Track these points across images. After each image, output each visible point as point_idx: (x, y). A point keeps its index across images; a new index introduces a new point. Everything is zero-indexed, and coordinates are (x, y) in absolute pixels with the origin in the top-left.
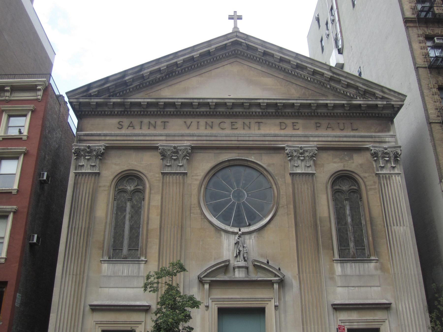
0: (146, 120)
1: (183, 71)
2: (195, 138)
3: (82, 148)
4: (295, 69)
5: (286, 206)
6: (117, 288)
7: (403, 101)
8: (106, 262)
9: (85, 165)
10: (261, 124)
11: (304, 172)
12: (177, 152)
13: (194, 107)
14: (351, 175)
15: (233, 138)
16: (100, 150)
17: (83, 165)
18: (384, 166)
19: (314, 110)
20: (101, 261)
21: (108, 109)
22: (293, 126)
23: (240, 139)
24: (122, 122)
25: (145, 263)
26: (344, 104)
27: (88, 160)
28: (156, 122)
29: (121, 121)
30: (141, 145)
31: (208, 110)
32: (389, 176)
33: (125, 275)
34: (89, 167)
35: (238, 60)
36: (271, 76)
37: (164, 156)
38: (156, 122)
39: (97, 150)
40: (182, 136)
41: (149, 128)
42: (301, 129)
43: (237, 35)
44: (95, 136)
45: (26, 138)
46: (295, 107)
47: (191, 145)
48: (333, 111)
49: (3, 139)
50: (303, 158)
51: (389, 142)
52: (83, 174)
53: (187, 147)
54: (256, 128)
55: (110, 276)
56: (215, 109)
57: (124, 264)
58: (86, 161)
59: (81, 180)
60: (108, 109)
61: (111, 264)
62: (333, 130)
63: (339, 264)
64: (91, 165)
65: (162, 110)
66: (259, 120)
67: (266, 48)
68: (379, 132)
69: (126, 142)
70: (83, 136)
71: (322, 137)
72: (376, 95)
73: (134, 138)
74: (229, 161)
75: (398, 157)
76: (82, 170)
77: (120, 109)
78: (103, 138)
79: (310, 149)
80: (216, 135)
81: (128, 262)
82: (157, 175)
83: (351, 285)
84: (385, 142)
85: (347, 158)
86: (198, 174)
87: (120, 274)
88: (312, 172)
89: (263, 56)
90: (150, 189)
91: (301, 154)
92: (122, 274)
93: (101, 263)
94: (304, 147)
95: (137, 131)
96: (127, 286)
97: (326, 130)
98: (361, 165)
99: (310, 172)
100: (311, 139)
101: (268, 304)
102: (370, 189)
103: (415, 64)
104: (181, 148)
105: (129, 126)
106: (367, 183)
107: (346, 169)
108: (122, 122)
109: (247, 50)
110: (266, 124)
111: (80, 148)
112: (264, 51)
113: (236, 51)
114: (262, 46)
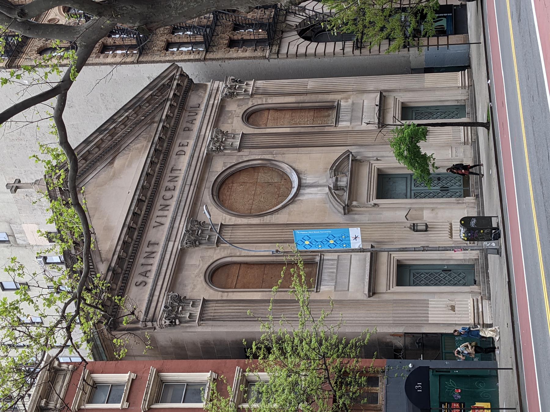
2: (179, 218)
4: (112, 139)
5: (274, 155)
7: (179, 67)
8: (319, 287)
15: (187, 188)
20: (317, 292)
22: (169, 190)
23: (189, 182)
26: (170, 105)
31: (146, 204)
33: (335, 270)
37: (218, 150)
40: (152, 295)
41: (166, 216)
45: (134, 375)
49: (127, 401)
50: (181, 307)
51: (219, 85)
52: (201, 313)
55: (336, 282)
57: (323, 272)
61: (322, 283)
64: (192, 306)
65: (123, 272)
69: (167, 277)
70: (147, 317)
71: (205, 115)
72: (166, 83)
73: (164, 269)
79: (214, 133)
82: (218, 251)
84: (218, 88)
86: (224, 218)
89: (86, 161)
95: (182, 174)
100: (203, 133)
102: (266, 101)
103: (132, 63)
110: (174, 165)
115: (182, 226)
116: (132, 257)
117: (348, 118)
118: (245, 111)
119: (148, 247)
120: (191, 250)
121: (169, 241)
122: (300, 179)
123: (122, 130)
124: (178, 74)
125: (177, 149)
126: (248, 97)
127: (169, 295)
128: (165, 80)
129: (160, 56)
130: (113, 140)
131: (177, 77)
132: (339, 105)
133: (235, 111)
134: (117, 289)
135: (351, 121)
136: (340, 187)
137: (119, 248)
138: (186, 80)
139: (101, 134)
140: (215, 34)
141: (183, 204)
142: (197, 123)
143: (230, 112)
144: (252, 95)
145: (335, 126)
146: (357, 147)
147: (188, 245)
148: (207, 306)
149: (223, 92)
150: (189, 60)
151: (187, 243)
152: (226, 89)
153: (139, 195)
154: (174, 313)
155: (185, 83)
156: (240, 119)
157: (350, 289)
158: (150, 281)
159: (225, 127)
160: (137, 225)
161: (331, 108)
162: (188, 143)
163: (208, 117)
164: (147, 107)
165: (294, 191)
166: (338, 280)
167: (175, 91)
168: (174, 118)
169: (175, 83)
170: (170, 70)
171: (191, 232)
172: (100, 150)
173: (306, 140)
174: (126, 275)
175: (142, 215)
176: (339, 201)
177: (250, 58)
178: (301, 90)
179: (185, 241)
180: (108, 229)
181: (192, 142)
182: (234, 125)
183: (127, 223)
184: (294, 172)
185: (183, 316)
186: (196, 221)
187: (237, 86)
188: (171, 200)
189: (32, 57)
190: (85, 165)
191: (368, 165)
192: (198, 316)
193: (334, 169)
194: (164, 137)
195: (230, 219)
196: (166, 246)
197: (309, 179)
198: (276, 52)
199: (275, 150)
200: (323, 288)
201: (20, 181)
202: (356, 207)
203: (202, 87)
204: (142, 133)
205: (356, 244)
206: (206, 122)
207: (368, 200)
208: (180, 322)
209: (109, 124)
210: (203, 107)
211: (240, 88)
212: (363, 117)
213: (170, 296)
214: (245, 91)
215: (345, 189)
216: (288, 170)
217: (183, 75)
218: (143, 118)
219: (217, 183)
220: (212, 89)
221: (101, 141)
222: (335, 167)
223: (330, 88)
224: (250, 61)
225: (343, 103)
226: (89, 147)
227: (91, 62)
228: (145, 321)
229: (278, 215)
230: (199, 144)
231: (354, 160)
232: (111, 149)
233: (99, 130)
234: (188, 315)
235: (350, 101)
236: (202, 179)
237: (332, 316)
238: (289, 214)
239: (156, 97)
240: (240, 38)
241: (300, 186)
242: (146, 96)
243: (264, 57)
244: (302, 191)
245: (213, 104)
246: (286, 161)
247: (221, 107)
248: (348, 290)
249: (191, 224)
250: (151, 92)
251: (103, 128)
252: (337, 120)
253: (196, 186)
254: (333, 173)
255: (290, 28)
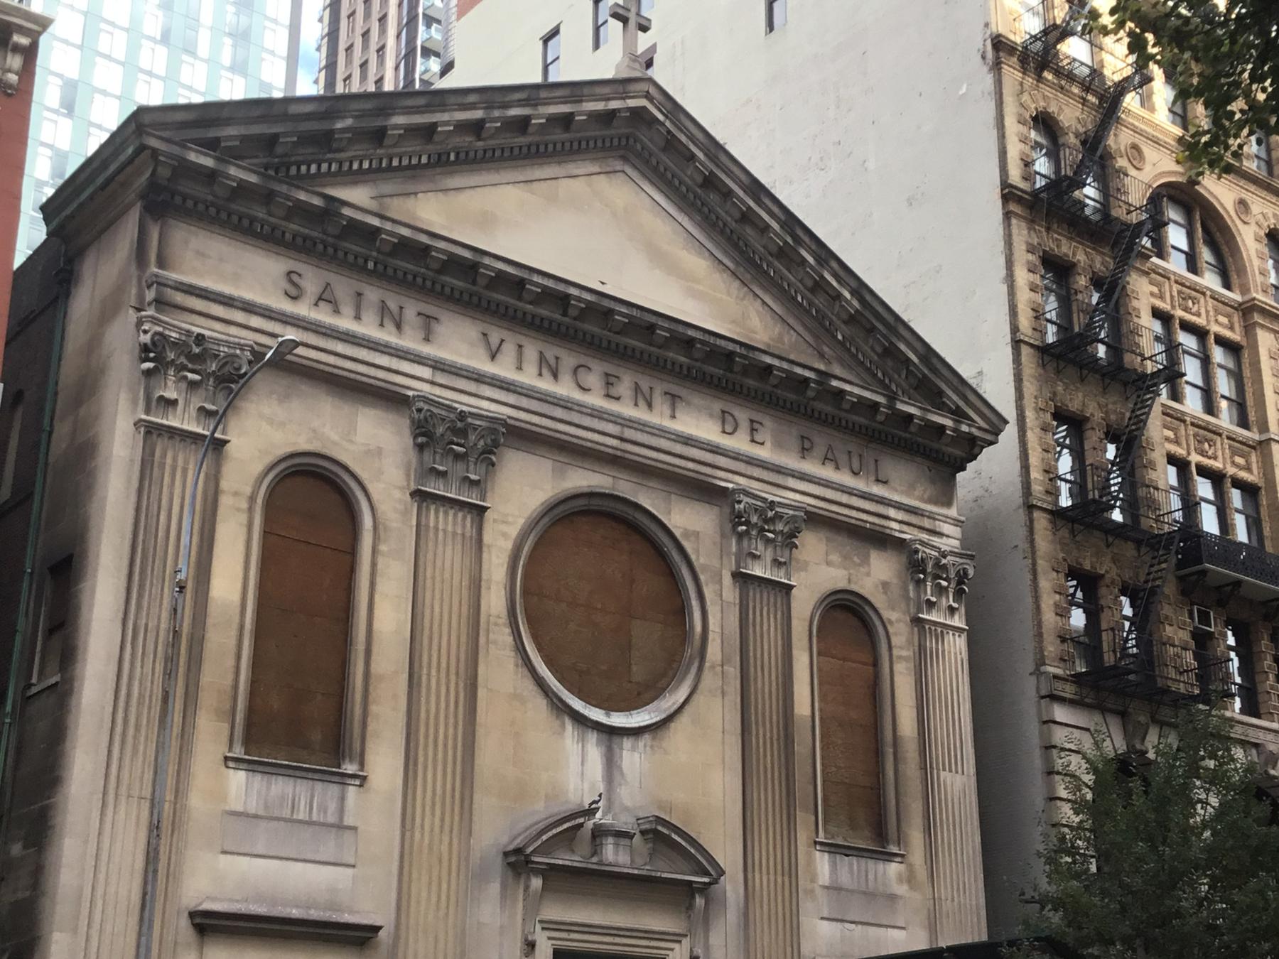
0: (373, 294)
1: (489, 154)
2: (511, 399)
3: (174, 335)
4: (771, 255)
5: (719, 669)
6: (281, 858)
7: (997, 435)
9: (181, 403)
10: (678, 400)
11: (770, 577)
12: (463, 433)
13: (525, 295)
14: (860, 606)
15: (611, 428)
16: (237, 360)
17: (173, 403)
18: (479, 481)
19: (809, 399)
20: (226, 758)
21: (266, 217)
22: (608, 384)
23: (629, 434)
24: (300, 275)
25: (361, 786)
27: (193, 385)
28: (401, 308)
29: (760, 420)
30: (359, 378)
31: (557, 316)
32: (942, 632)
33: (301, 817)
34: (194, 413)
35: (629, 170)
36: (707, 254)
37: (737, 518)
38: (401, 308)
39: (224, 357)
42: (768, 444)
43: (648, 92)
44: (214, 301)
46: (216, 188)
47: (255, 346)
48: (578, 324)
51: (948, 536)
52: (173, 432)
53: (496, 426)
54: (667, 411)
55: (256, 816)
56: (575, 319)
58: (183, 385)
59: (164, 456)
60: (266, 217)
62: (837, 468)
63: (826, 855)
64: (201, 409)
66: (675, 389)
67: (717, 166)
68: (930, 501)
72: (945, 400)
73: (340, 347)
74: (591, 495)
75: (964, 583)
76: (170, 418)
77: (306, 231)
78: (239, 316)
79: (791, 512)
80: (569, 405)
81: (310, 775)
82: (397, 494)
83: (849, 919)
84: (940, 534)
85: (856, 559)
86: (510, 519)
87: (286, 813)
88: (786, 581)
89: (701, 186)
90: (376, 539)
91: (767, 521)
92: (292, 812)
93: (227, 767)
94: (779, 503)
96: (309, 857)
97: (316, 304)
98: (885, 585)
99: (782, 580)
100: (792, 483)
101: (672, 950)
102: (900, 657)
103: (1015, 329)
104: (478, 423)
105: (320, 299)
106: (895, 641)
107: (854, 587)
108: (300, 275)
109: (664, 150)
110: (688, 404)
111: (167, 332)
112: (711, 172)
113: (631, 141)
114: (706, 155)
115: (489, 404)
116: (380, 267)
117: (845, 879)
118: (346, 468)
119: (419, 314)
120: (405, 424)
121: (434, 368)
122: (636, 732)
123: (801, 281)
124: (975, 431)
125: (742, 415)
126: (913, 610)
127: (242, 350)
128: (955, 397)
129: (1036, 397)
130: (770, 258)
131: (965, 428)
132: (886, 857)
133: (868, 574)
134: (272, 220)
135: (834, 888)
136: (602, 844)
137: (405, 232)
138: (958, 452)
139: (781, 227)
140: (1110, 539)
141: (559, 413)
142: (828, 473)
143: (866, 560)
144: (917, 621)
145: (816, 843)
146: (742, 905)
147: (416, 415)
148: (441, 509)
149: (923, 543)
150: (1025, 468)
151: (419, 410)
152: (936, 554)
153: (579, 299)
154: (183, 360)
155: (950, 450)
156: (842, 584)
157: (229, 857)
158: (303, 309)
159: (812, 545)
160: (487, 287)
161: (881, 834)
162: (762, 444)
163: (749, 473)
164: (873, 349)
165: (596, 714)
166: (263, 824)
167: (922, 419)
168: (837, 412)
169: (948, 422)
170: (986, 411)
171: (459, 424)
172: (736, 221)
173: (768, 757)
174: (320, 247)
175: (520, 304)
176: (544, 838)
177: (1039, 624)
178: (938, 752)
179: (426, 407)
180: (486, 221)
181: (763, 453)
182: (824, 567)
183: (487, 261)
184: (658, 719)
185: (170, 383)
186: (496, 444)
187: (944, 583)
188: (573, 385)
189: (1025, 97)
190: (689, 182)
191: (677, 931)
192: (165, 422)
193: (660, 828)
194: (773, 381)
195: (504, 535)
196: (419, 360)
197: (632, 757)
198: (1055, 692)
199: (733, 671)
200: (238, 779)
201: (644, 29)
202: (527, 888)
203: (946, 494)
204: (795, 334)
205: (1159, 758)
206: (829, 494)
207: (548, 926)
208: (148, 373)
209: (814, 247)
210: (877, 490)
211: (941, 591)
212: (847, 925)
213: (238, 352)
214: (928, 601)
215: (594, 860)
216: (670, 704)
217: (971, 448)
218: (840, 337)
219: (630, 511)
220: (935, 519)
221: (762, 225)
222: (665, 831)
223: (944, 835)
224: (1029, 625)
225: (894, 868)
226: (741, 193)
227: (1015, 231)
228: (161, 284)
229: (511, 666)
230: (757, 472)
231: (704, 889)
232: (744, 252)
233: (791, 221)
234: (171, 394)
235: (902, 890)
236: (644, 471)
237: (123, 800)
238: (515, 696)
239: (905, 371)
240: (1102, 602)
241: (611, 733)
242: (902, 347)
243: (1041, 662)
244: (592, 737)
245: (887, 518)
246: (699, 699)
247: (880, 539)
248: (224, 852)
249: (489, 428)
250: (915, 359)
251: (800, 233)
252: (833, 849)
253: (619, 453)
254: (647, 826)
255: (1134, 732)
